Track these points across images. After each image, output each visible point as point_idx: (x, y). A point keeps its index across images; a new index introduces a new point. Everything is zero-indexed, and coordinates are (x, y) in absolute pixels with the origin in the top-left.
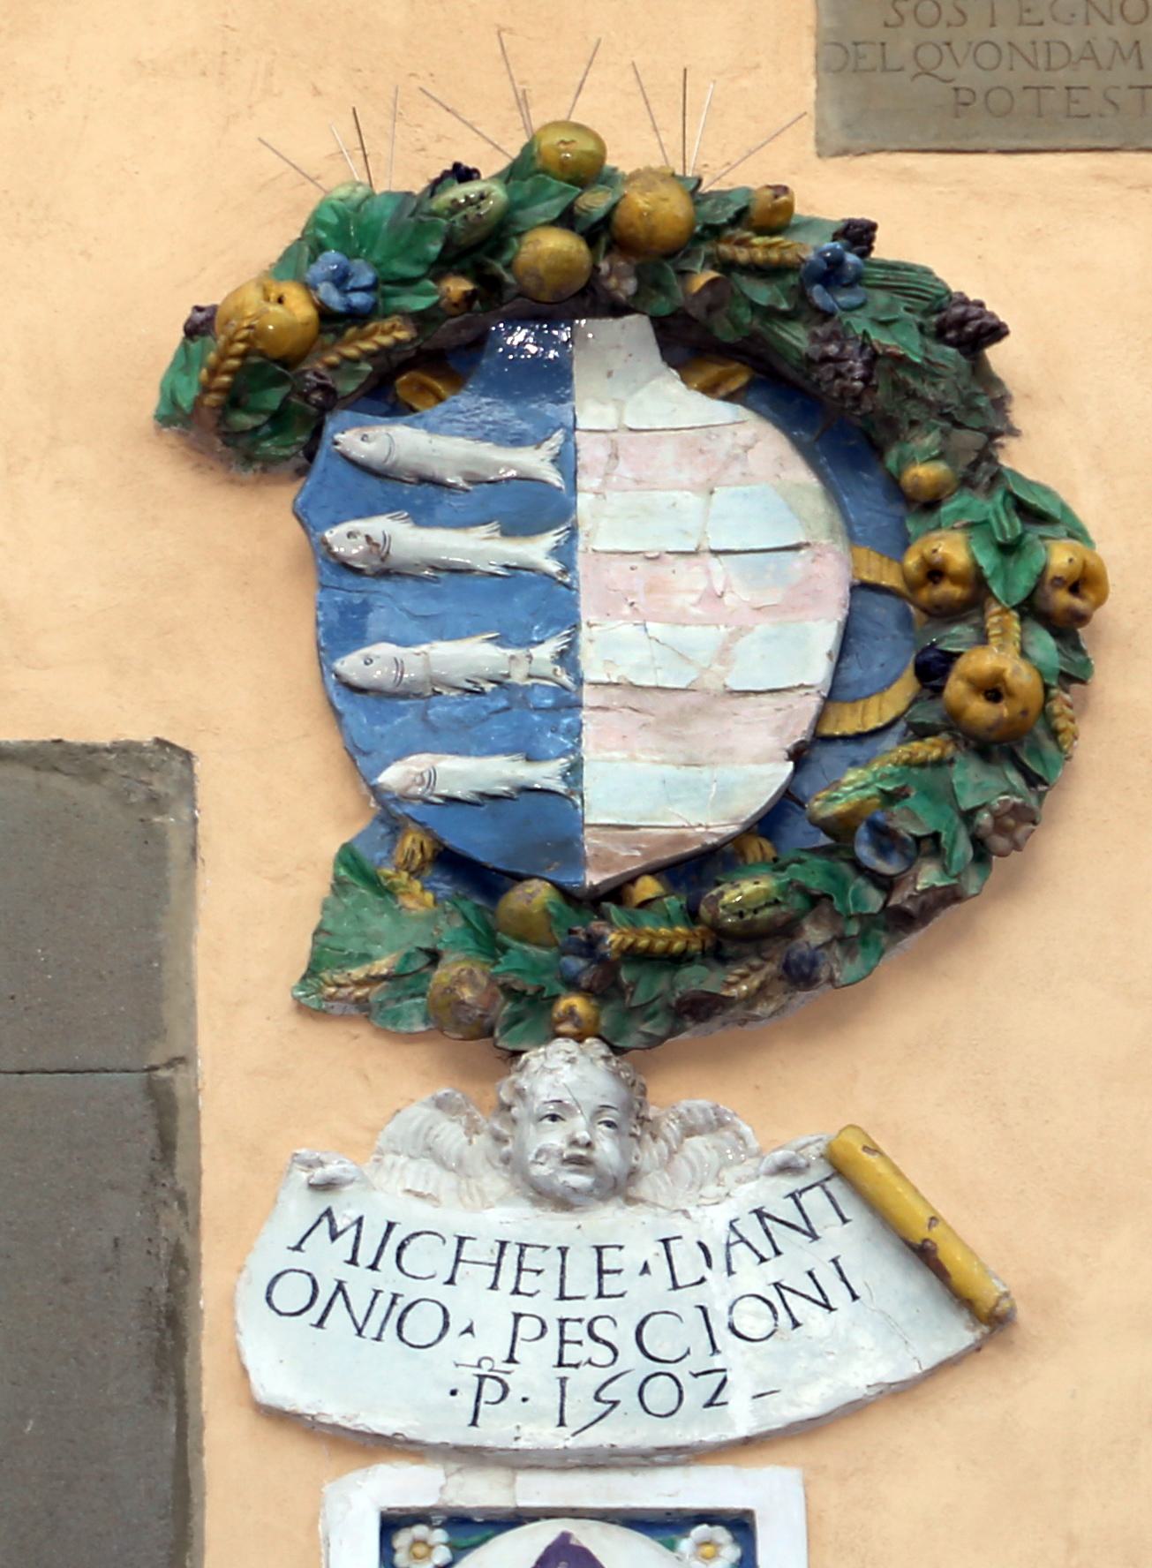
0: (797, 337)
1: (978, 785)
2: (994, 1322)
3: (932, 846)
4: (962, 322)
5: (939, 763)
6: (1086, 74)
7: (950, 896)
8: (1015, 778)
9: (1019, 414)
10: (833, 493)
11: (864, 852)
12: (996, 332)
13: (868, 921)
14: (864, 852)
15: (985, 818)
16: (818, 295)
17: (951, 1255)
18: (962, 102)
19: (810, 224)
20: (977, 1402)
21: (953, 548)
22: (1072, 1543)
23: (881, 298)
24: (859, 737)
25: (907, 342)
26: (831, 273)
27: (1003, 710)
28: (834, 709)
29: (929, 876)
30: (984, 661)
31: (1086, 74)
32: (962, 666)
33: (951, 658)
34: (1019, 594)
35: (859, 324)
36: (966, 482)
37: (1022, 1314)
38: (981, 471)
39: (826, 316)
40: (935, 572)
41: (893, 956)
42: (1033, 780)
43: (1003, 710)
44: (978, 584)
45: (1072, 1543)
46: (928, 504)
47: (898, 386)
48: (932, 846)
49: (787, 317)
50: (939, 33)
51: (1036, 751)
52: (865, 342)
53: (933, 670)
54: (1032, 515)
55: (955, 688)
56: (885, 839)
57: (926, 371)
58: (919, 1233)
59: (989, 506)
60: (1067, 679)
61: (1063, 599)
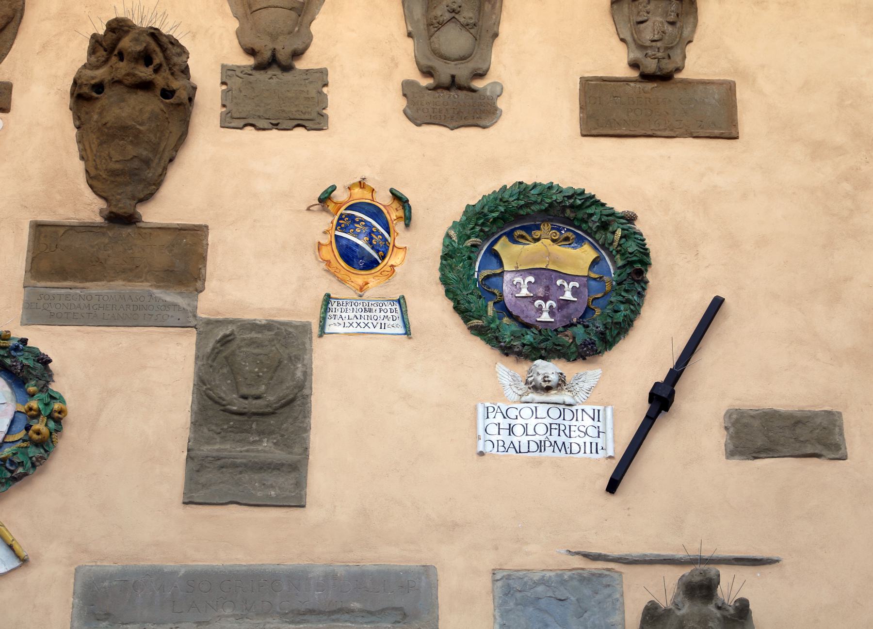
0: (8, 361)
1: (33, 452)
2: (24, 561)
3: (21, 464)
4: (42, 359)
5: (26, 447)
6: (78, 310)
7: (25, 474)
8: (42, 451)
9: (55, 378)
10: (14, 392)
11: (8, 465)
12: (50, 361)
13: (7, 480)
14: (8, 465)
15: (34, 459)
16: (13, 353)
17: (16, 547)
18: (52, 315)
19: (14, 338)
20: (18, 578)
21: (34, 404)
22: (35, 606)
23: (27, 354)
24: (13, 442)
25: (30, 363)
26: (16, 349)
27: (40, 437)
28: (8, 436)
29: (20, 470)
30: (36, 427)
31: (78, 310)
32: (33, 428)
33: (31, 426)
34: (48, 413)
35: (21, 359)
36: (41, 391)
37: (31, 559)
38: (44, 388)
39: (14, 357)
40: (31, 409)
41: (13, 486)
42: (46, 451)
43: (40, 437)
44: (39, 411)
45: (35, 606)
46: (32, 395)
47: (28, 371)
48: (21, 464)
49: (6, 357)
50: (49, 301)
51: (48, 445)
52: (21, 362)
53: (28, 428)
54: (53, 398)
55: (31, 432)
56: (12, 463)
57: (34, 369)
58: (10, 543)
59: (43, 396)
60: (57, 431)
61: (56, 415)
